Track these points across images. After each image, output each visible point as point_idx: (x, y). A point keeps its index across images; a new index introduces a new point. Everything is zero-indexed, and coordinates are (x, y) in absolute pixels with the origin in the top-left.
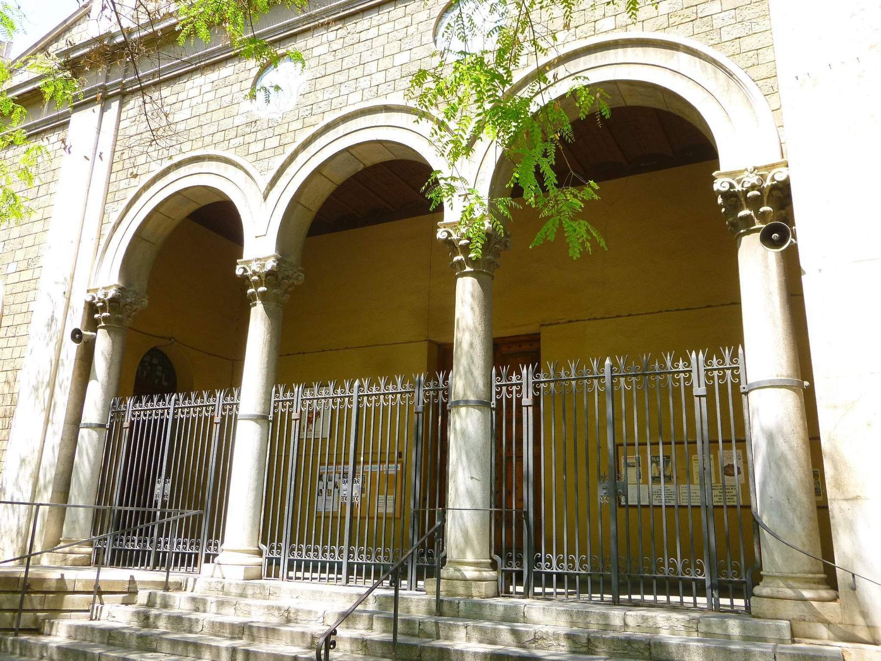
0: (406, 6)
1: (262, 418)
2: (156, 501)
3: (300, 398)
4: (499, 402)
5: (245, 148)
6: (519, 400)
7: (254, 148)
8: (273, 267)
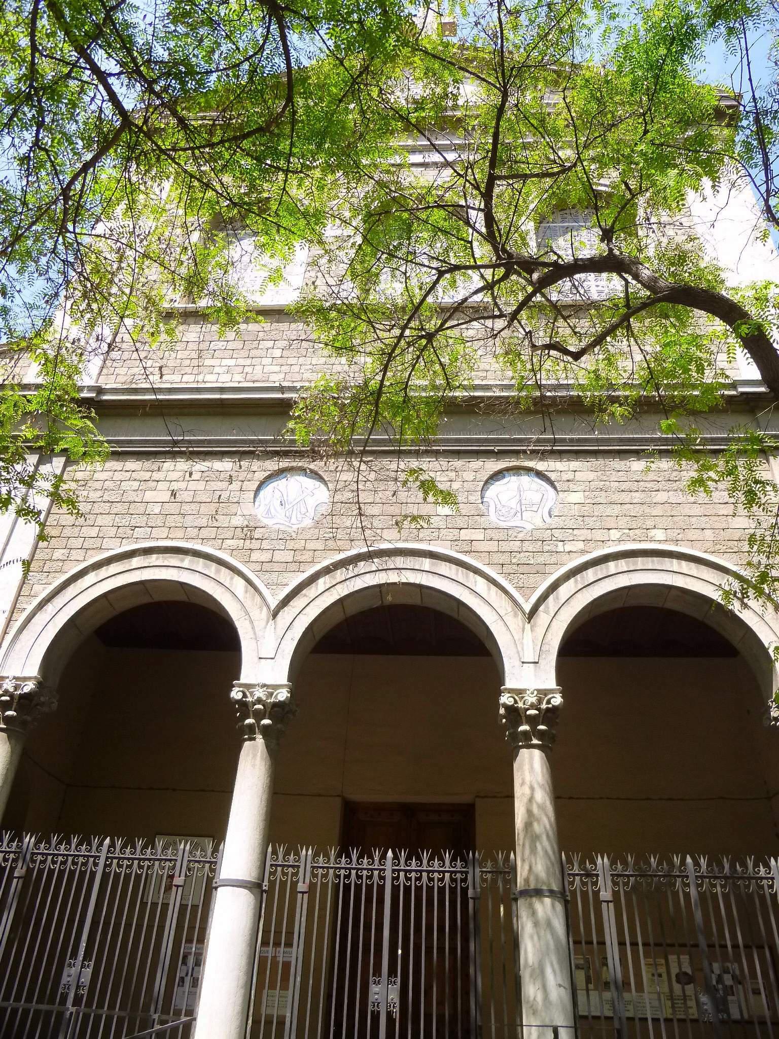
0: (449, 462)
1: (255, 887)
2: (373, 1012)
3: (186, 859)
4: (272, 883)
5: (246, 554)
6: (294, 884)
7: (256, 556)
8: (287, 697)
